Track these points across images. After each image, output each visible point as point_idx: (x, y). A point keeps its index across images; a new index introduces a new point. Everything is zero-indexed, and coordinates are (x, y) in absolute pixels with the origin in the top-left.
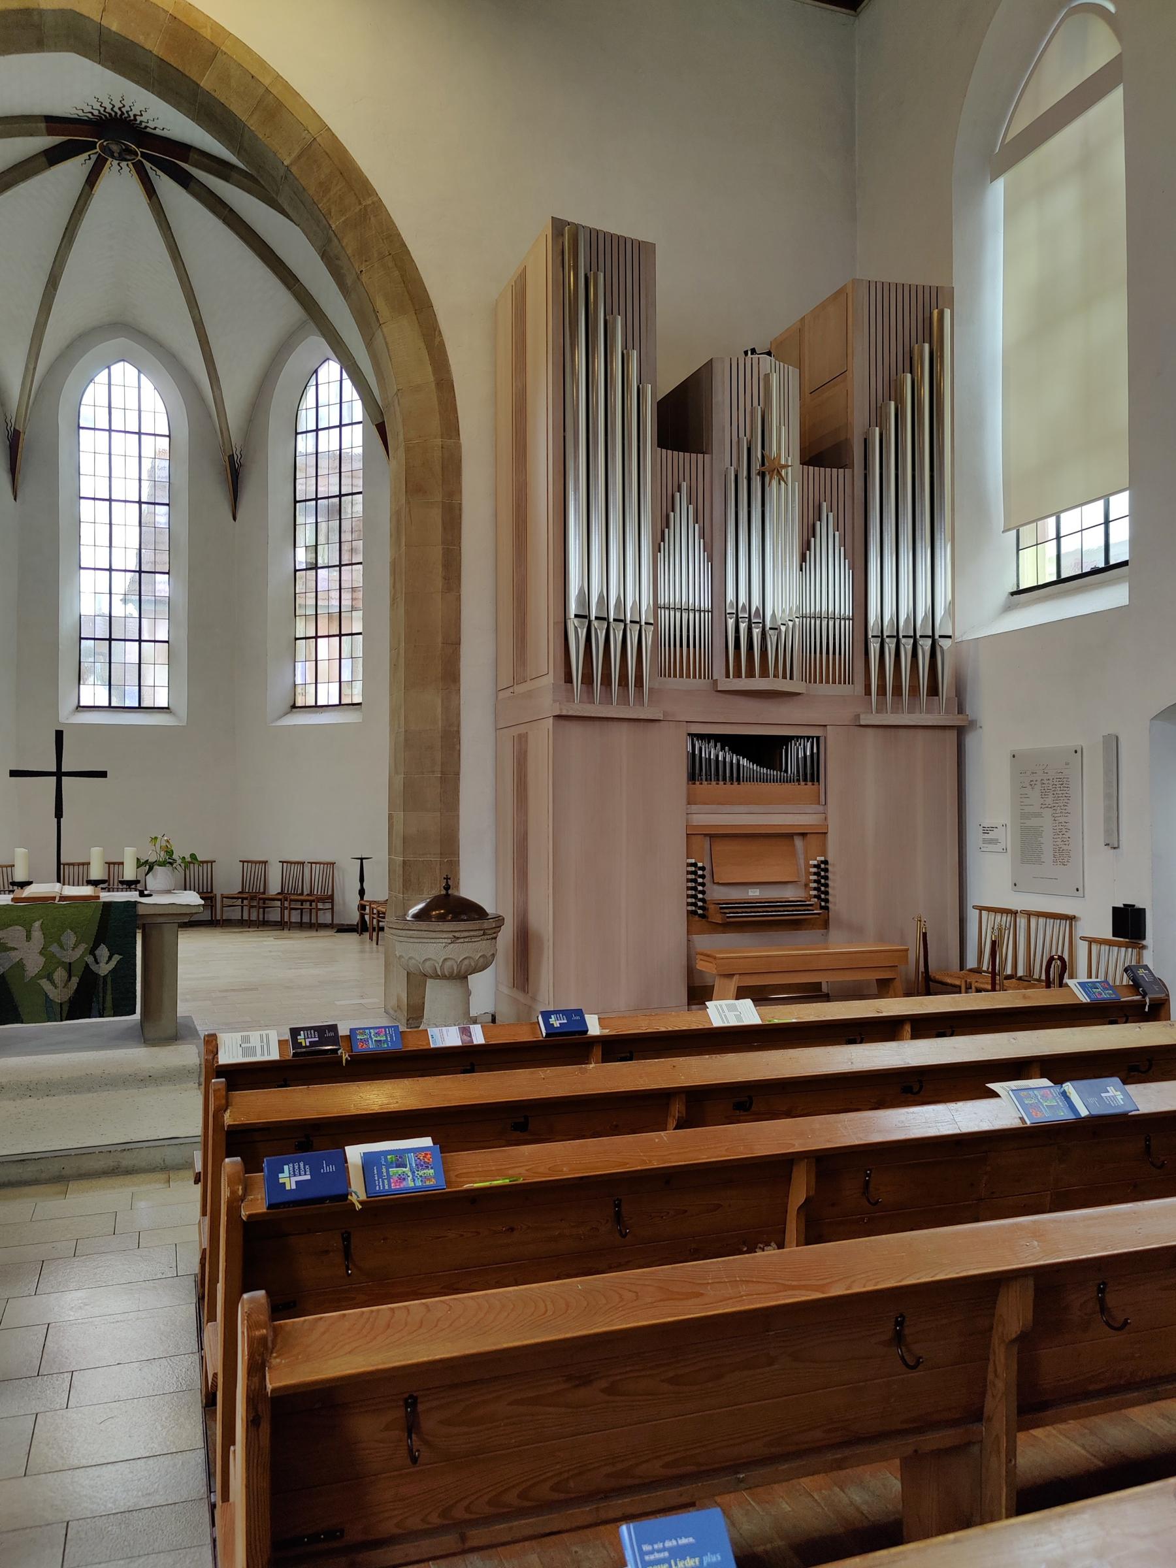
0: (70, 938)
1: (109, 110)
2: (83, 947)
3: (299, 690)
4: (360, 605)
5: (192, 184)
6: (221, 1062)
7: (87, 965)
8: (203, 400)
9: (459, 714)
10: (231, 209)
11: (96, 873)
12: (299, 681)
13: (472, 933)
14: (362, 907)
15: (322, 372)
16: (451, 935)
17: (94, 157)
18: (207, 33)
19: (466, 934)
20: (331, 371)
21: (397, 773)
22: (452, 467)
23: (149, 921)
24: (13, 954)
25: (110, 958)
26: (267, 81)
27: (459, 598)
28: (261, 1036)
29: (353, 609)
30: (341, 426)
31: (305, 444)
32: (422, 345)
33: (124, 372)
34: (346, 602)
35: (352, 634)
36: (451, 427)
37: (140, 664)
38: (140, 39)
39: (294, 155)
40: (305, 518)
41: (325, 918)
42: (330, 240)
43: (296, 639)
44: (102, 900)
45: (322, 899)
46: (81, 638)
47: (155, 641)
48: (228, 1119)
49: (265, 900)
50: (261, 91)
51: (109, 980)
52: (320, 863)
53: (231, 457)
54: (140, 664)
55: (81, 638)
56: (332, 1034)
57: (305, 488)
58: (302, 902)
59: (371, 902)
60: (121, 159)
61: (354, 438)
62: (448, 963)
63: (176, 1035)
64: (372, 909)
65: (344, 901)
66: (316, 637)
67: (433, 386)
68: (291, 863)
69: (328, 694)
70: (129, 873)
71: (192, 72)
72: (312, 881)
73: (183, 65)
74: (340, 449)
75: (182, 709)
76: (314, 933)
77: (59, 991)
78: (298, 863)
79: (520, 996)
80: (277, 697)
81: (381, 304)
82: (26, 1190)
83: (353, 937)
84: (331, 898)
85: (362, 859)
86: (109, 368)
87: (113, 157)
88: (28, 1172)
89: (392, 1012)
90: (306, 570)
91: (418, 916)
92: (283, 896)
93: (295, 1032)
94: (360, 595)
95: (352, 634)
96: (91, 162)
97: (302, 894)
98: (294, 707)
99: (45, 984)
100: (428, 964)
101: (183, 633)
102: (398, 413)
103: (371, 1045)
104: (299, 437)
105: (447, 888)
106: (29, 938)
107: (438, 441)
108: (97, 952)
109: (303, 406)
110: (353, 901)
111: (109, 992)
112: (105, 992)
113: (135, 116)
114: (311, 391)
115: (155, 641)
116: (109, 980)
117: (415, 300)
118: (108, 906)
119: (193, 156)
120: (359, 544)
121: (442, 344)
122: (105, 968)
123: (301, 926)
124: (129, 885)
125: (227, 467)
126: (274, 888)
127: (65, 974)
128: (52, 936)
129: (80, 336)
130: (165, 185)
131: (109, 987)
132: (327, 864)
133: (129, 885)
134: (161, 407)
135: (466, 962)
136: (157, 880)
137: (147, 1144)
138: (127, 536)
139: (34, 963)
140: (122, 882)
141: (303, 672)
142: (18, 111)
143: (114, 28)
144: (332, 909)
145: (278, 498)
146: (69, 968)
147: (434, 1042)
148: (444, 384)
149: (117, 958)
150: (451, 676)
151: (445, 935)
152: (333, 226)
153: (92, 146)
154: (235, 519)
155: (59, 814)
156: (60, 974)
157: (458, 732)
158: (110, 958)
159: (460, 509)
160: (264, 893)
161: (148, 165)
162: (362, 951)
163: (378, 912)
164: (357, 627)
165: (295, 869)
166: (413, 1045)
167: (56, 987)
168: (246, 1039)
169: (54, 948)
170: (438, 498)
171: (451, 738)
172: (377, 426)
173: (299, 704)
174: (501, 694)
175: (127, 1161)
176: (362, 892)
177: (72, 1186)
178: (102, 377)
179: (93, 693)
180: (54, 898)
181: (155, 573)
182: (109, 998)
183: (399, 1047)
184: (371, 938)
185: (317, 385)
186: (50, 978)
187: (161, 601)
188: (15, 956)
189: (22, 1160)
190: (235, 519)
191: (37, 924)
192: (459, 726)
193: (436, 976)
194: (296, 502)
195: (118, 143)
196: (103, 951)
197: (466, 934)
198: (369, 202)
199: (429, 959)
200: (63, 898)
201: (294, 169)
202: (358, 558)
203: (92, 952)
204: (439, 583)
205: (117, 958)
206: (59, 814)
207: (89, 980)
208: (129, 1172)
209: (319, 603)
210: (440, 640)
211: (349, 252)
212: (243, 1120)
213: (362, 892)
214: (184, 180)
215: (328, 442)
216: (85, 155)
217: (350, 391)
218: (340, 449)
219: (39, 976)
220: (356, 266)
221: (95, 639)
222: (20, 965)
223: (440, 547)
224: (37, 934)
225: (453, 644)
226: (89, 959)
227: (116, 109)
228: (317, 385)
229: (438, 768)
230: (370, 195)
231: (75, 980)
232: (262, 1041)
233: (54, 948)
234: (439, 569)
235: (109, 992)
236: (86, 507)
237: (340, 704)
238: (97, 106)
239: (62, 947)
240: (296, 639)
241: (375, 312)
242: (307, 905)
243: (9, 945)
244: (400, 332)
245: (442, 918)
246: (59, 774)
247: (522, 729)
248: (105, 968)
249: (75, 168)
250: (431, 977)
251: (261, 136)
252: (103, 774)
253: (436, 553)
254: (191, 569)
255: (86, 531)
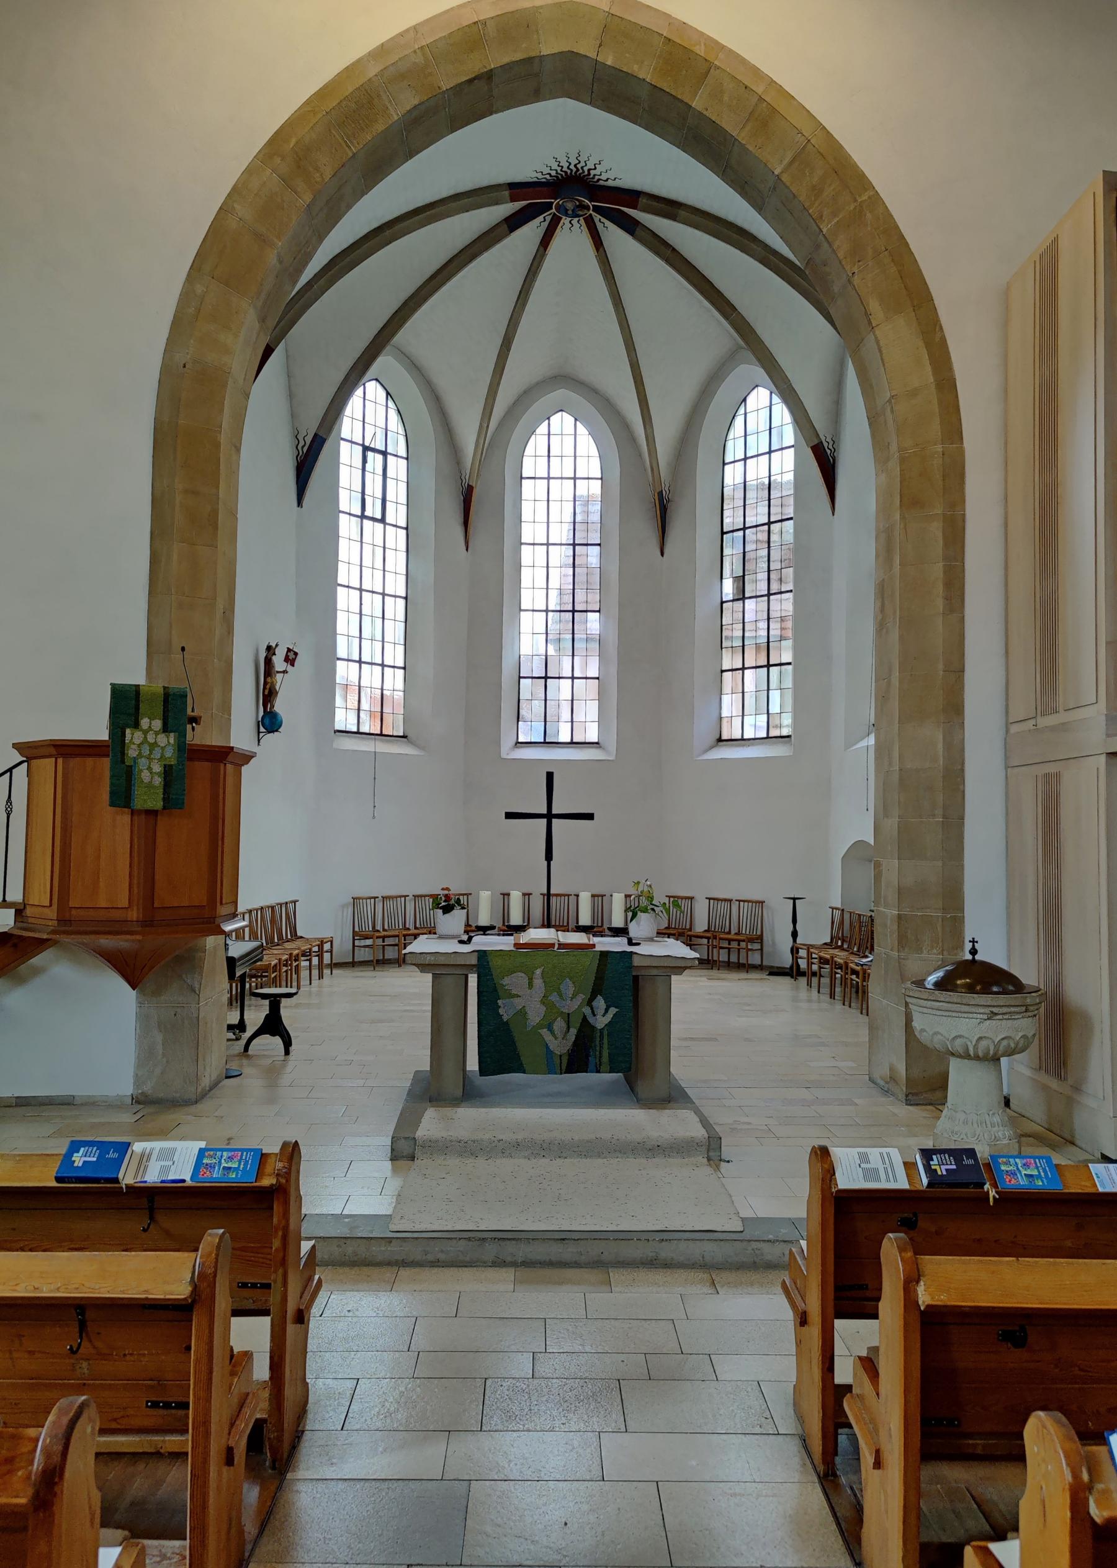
0: (569, 988)
1: (565, 169)
2: (581, 997)
3: (724, 721)
4: (789, 633)
5: (638, 231)
6: (841, 1186)
7: (585, 1017)
8: (633, 439)
9: (963, 750)
10: (674, 249)
11: (585, 919)
12: (725, 713)
13: (1013, 1009)
14: (794, 951)
15: (751, 400)
16: (987, 1010)
17: (548, 219)
18: (700, 50)
19: (1005, 1010)
20: (760, 398)
21: (886, 814)
22: (954, 473)
23: (643, 972)
24: (516, 1000)
25: (606, 1011)
26: (760, 90)
27: (962, 620)
28: (881, 1154)
29: (782, 638)
30: (770, 452)
31: (733, 475)
32: (921, 344)
33: (563, 422)
34: (775, 632)
35: (781, 664)
36: (953, 431)
37: (572, 700)
38: (635, 69)
39: (785, 162)
40: (732, 551)
41: (755, 959)
42: (818, 246)
43: (722, 671)
44: (598, 948)
45: (751, 940)
46: (520, 677)
47: (586, 678)
48: (924, 1296)
49: (691, 936)
50: (755, 100)
51: (605, 1032)
52: (748, 901)
53: (660, 493)
54: (572, 700)
55: (520, 677)
56: (971, 1162)
57: (731, 519)
58: (730, 941)
59: (809, 947)
60: (575, 215)
61: (785, 466)
62: (984, 1043)
63: (672, 1097)
64: (809, 954)
65: (773, 940)
66: (743, 669)
67: (933, 386)
68: (718, 900)
69: (755, 726)
70: (618, 921)
71: (684, 94)
72: (739, 920)
73: (669, 91)
74: (745, 482)
75: (611, 743)
76: (743, 975)
77: (560, 1043)
78: (725, 900)
79: (1054, 1084)
80: (703, 731)
81: (874, 306)
82: (570, 1273)
83: (786, 981)
84: (760, 939)
85: (794, 899)
86: (549, 418)
87: (567, 215)
88: (568, 1252)
89: (882, 1083)
90: (733, 601)
91: (940, 985)
92: (711, 934)
93: (927, 1154)
94: (789, 624)
95: (781, 664)
96: (546, 224)
97: (729, 933)
98: (720, 740)
99: (544, 1032)
100: (959, 1041)
101: (613, 670)
102: (890, 422)
103: (1023, 1182)
104: (726, 467)
105: (974, 952)
106: (531, 985)
107: (939, 448)
108: (594, 1004)
109: (731, 436)
110: (784, 943)
111: (606, 1046)
112: (601, 1047)
113: (589, 170)
114: (739, 421)
115: (586, 678)
116: (605, 1032)
117: (915, 296)
118: (604, 955)
119: (643, 201)
120: (789, 573)
121: (943, 341)
122: (601, 1021)
123: (729, 966)
124: (621, 932)
125: (658, 500)
126: (700, 926)
127: (564, 1025)
128: (553, 986)
129: (525, 392)
130: (612, 233)
131: (605, 1041)
132: (756, 902)
133: (621, 932)
134: (594, 451)
135: (1005, 1043)
136: (642, 927)
137: (687, 1235)
138: (560, 577)
139: (536, 1013)
140: (610, 929)
141: (729, 705)
142: (485, 183)
143: (609, 63)
144: (762, 949)
145: (706, 532)
146: (568, 1018)
147: (1103, 1185)
148: (946, 384)
149: (613, 1011)
150: (953, 708)
151: (982, 1010)
152: (825, 230)
153: (549, 206)
154: (662, 555)
155: (549, 856)
156: (559, 1025)
157: (963, 770)
158: (606, 1011)
159: (964, 521)
160: (690, 930)
161: (597, 217)
162: (795, 999)
163: (821, 958)
164: (787, 657)
165: (722, 907)
166: (1075, 1187)
167: (556, 1038)
168: (864, 1158)
169: (554, 997)
170: (939, 510)
171: (954, 776)
172: (812, 448)
173: (724, 737)
174: (1014, 729)
175: (666, 1252)
176: (795, 934)
177: (615, 1275)
178: (543, 428)
179: (529, 732)
180: (553, 945)
181: (586, 611)
182: (605, 1053)
183: (1057, 1187)
184: (809, 984)
185: (745, 414)
186: (550, 1028)
187: (592, 639)
188: (518, 1003)
189: (563, 1238)
190: (662, 555)
191: (538, 972)
192: (963, 764)
193: (966, 1056)
194: (723, 533)
195: (572, 199)
196: (600, 1003)
197: (1005, 1010)
198: (865, 197)
199: (960, 1036)
200: (562, 946)
201: (785, 178)
202: (790, 512)
203: (590, 1003)
204: (940, 604)
205: (613, 1011)
206: (549, 856)
207: (586, 1032)
208: (668, 1265)
209: (746, 634)
210: (941, 666)
211: (841, 255)
212: (943, 1299)
213: (795, 934)
214: (630, 226)
215: (757, 471)
216: (541, 218)
217: (782, 414)
218: (745, 482)
219: (540, 1026)
220: (848, 268)
221: (533, 678)
222: (522, 1013)
223: (941, 564)
224: (538, 982)
225: (956, 671)
226: (587, 1011)
227: (572, 167)
228: (745, 414)
229: (939, 812)
230: (866, 190)
231: (573, 1032)
232: (884, 1163)
233: (554, 997)
234: (940, 589)
235: (606, 1046)
236: (526, 552)
237: (768, 737)
238: (555, 166)
239: (561, 996)
240: (722, 671)
241: (867, 314)
242: (734, 945)
243: (514, 992)
244: (895, 336)
245: (970, 989)
246: (549, 816)
247: (1051, 768)
248: (601, 1021)
249: (533, 230)
250: (960, 1056)
251: (751, 149)
252: (590, 817)
253: (937, 571)
254: (621, 606)
255: (526, 574)
